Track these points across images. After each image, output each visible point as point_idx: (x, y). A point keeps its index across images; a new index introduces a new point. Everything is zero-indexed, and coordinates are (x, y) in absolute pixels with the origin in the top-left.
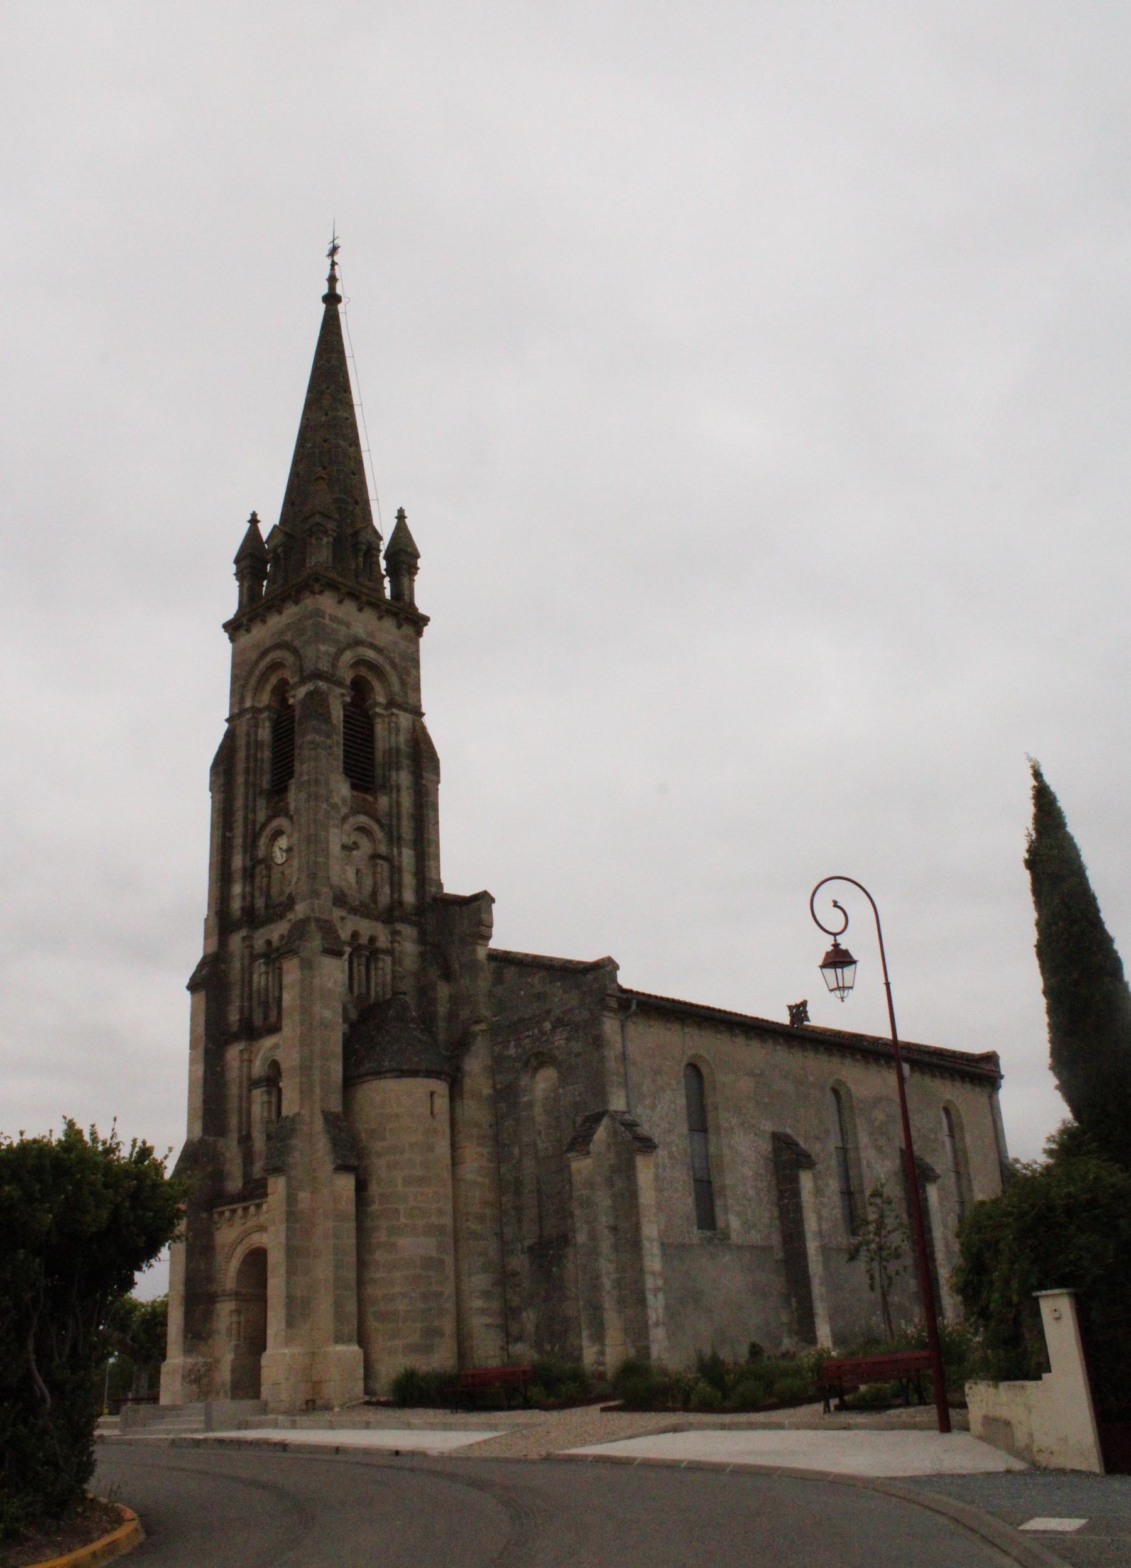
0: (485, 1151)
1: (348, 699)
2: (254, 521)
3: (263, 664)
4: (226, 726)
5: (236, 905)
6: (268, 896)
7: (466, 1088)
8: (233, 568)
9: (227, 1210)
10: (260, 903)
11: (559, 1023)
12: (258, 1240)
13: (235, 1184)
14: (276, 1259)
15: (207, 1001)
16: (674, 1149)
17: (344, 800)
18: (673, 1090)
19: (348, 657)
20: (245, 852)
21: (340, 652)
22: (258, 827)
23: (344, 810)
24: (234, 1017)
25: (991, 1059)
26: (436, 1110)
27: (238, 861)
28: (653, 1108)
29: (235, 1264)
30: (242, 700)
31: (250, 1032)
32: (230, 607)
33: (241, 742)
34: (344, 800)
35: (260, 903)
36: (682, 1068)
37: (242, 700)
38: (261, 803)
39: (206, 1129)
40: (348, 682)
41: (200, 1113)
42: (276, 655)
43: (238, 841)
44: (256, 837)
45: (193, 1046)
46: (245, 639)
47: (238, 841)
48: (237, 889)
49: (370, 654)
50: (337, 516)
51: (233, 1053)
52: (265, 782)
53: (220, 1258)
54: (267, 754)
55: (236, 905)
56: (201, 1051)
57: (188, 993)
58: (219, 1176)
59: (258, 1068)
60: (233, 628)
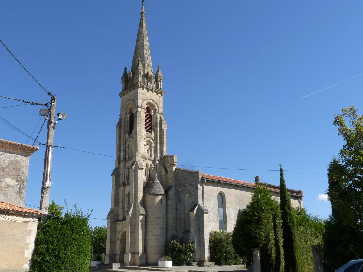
0: (311, 216)
1: (146, 112)
2: (126, 69)
3: (127, 103)
4: (124, 70)
5: (122, 157)
6: (129, 155)
7: (169, 197)
8: (121, 81)
9: (119, 223)
10: (127, 157)
11: (189, 184)
12: (125, 229)
13: (121, 218)
14: (128, 234)
15: (116, 178)
16: (214, 212)
17: (144, 134)
18: (215, 199)
19: (146, 102)
20: (124, 146)
21: (144, 101)
22: (126, 140)
23: (144, 137)
24: (121, 181)
25: (300, 192)
26: (162, 202)
27: (122, 148)
28: (210, 203)
29: (120, 234)
30: (123, 111)
31: (124, 184)
32: (120, 90)
33: (123, 121)
34: (144, 134)
35: (127, 157)
36: (218, 194)
37: (123, 111)
38: (127, 135)
39: (115, 206)
40: (146, 108)
41: (114, 202)
42: (130, 101)
43: (122, 143)
44: (126, 142)
45: (112, 188)
46: (123, 97)
47: (122, 143)
48: (122, 154)
49: (151, 101)
50: (143, 70)
51: (121, 189)
52: (128, 130)
53: (118, 233)
54: (128, 123)
55: (122, 157)
56: (114, 189)
57: (111, 176)
58: (117, 215)
59: (126, 193)
60: (121, 94)
